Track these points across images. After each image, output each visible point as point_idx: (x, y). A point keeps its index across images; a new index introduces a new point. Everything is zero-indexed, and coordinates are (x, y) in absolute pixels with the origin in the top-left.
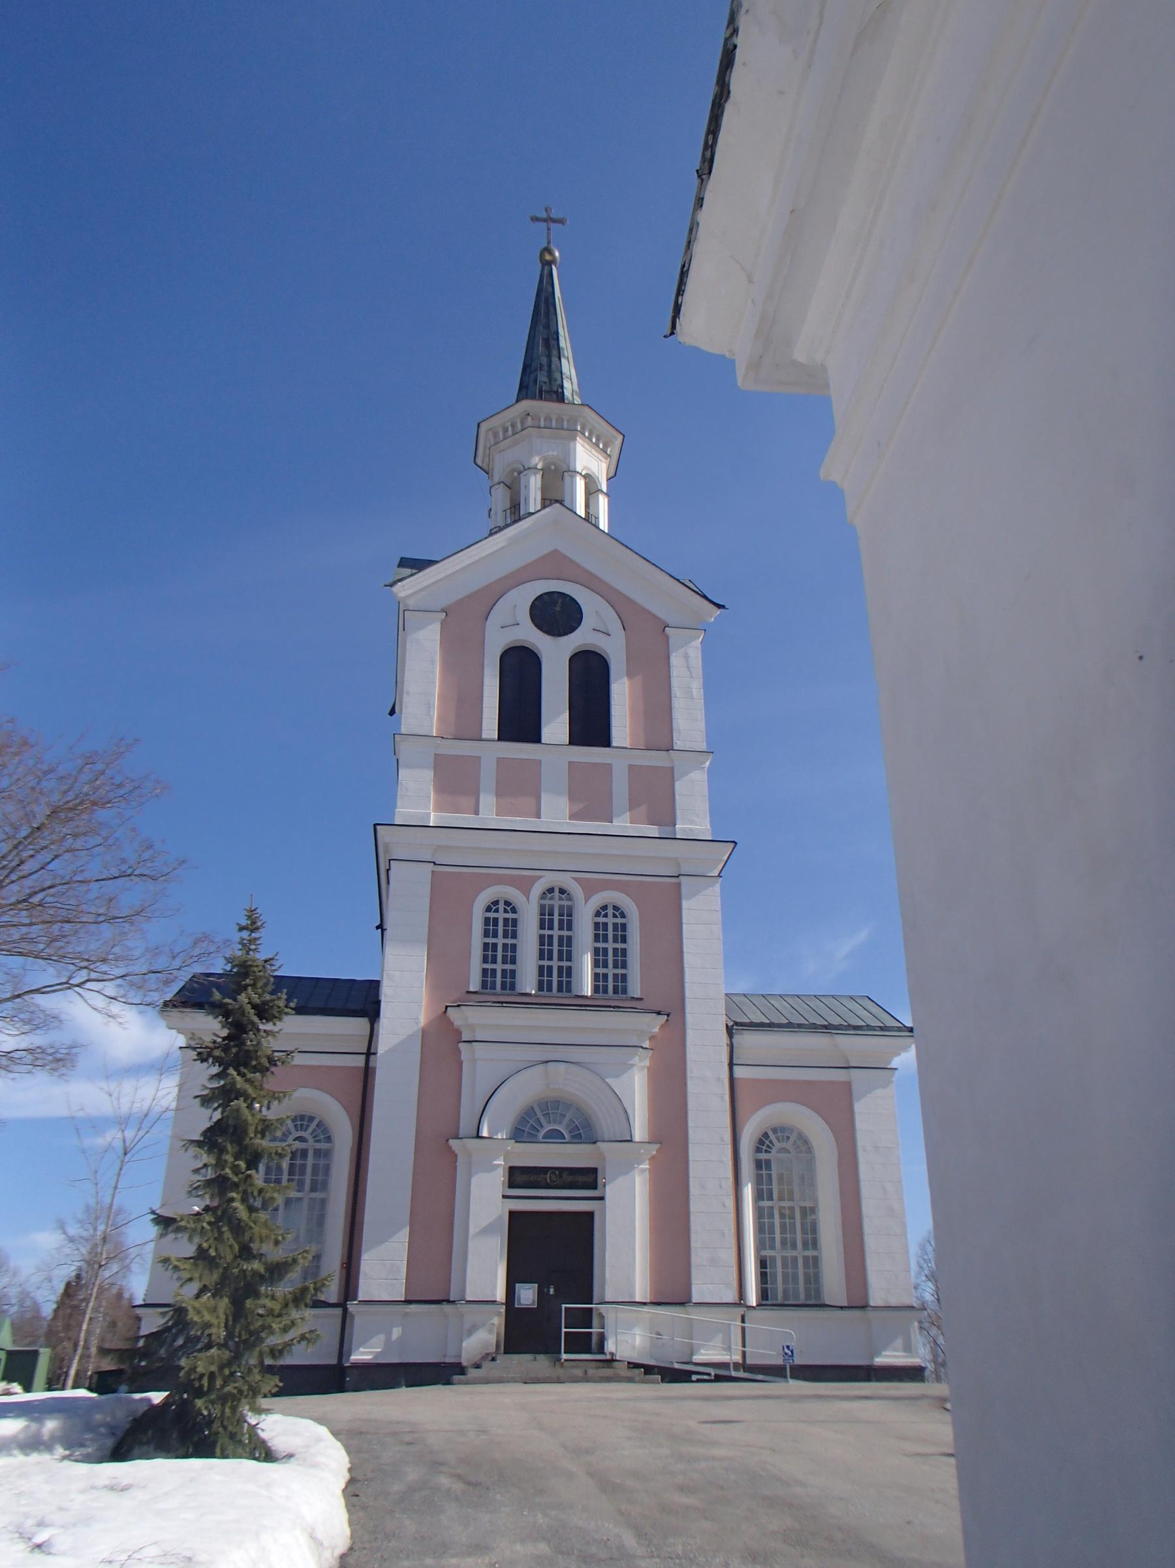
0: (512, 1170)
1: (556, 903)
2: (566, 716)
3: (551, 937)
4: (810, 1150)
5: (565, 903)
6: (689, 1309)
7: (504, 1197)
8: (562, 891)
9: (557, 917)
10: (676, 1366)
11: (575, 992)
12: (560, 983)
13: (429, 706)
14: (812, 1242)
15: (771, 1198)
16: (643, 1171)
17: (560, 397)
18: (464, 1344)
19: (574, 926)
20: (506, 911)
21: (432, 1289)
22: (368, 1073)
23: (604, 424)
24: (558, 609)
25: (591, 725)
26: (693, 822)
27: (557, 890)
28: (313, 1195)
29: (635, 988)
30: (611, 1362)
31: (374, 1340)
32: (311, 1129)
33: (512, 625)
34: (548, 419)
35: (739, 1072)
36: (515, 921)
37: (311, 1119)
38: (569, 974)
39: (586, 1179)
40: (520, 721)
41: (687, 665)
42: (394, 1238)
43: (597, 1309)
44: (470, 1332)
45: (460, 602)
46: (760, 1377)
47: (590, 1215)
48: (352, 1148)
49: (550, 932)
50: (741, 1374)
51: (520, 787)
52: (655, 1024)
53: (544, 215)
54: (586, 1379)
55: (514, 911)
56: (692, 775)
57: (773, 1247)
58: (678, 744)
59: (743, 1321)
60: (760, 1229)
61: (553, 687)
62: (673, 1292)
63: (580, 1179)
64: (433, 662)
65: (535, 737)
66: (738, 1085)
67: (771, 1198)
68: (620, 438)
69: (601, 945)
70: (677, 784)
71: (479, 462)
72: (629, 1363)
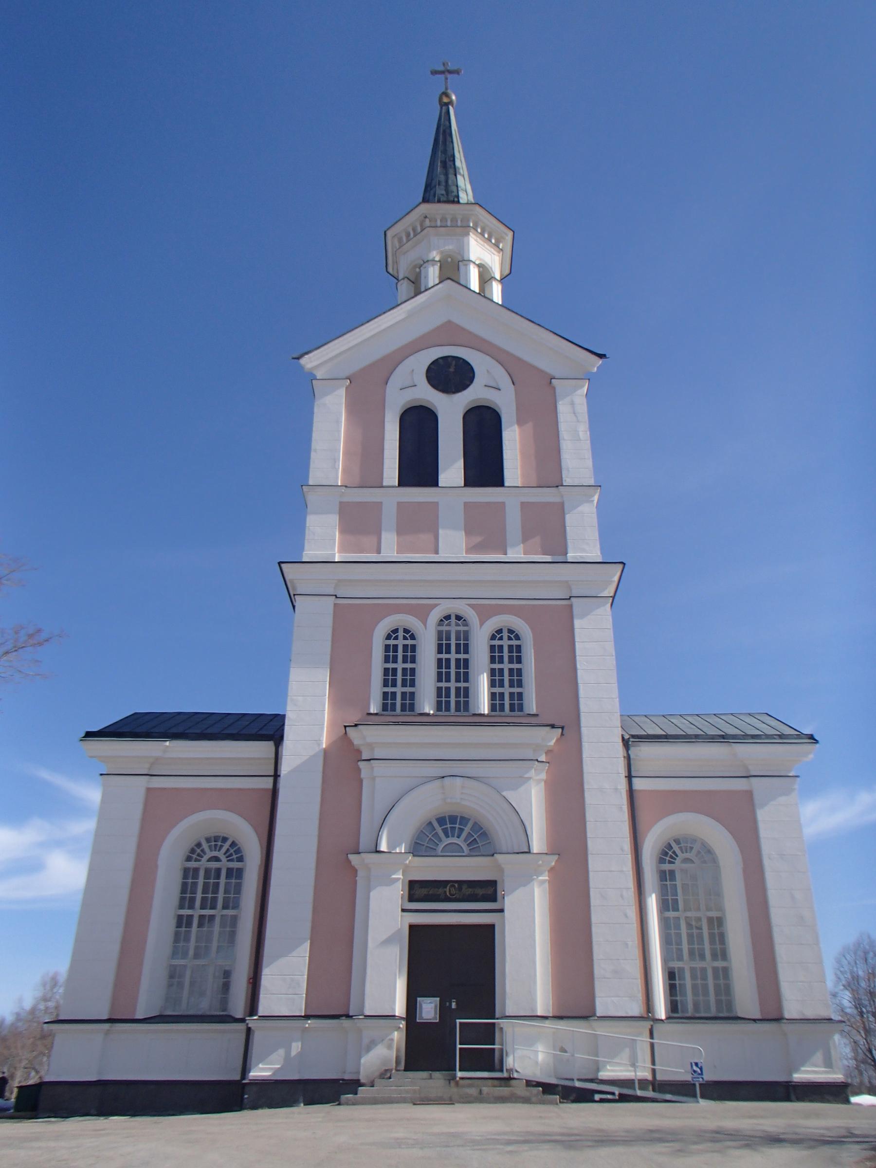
0: (412, 884)
1: (453, 629)
2: (461, 463)
3: (448, 689)
4: (715, 861)
5: (462, 628)
6: (595, 1024)
7: (403, 910)
8: (458, 618)
9: (454, 645)
10: (578, 1084)
11: (472, 710)
12: (458, 703)
13: (335, 460)
14: (722, 953)
15: (676, 909)
16: (543, 882)
17: (456, 201)
18: (363, 1061)
19: (471, 649)
20: (405, 638)
21: (333, 1003)
22: (275, 792)
23: (495, 222)
24: (452, 370)
25: (484, 467)
26: (584, 550)
27: (453, 617)
28: (225, 912)
29: (531, 704)
30: (508, 1080)
31: (274, 1056)
32: (224, 849)
33: (411, 386)
34: (444, 219)
35: (638, 784)
36: (414, 647)
37: (225, 839)
38: (466, 695)
39: (486, 891)
40: (419, 467)
41: (573, 413)
42: (294, 953)
43: (499, 1024)
44: (369, 1049)
45: (364, 370)
46: (668, 1097)
47: (491, 927)
48: (260, 866)
49: (447, 656)
50: (650, 1094)
51: (420, 524)
52: (551, 738)
53: (441, 68)
54: (481, 1099)
55: (413, 637)
56: (580, 508)
57: (680, 958)
58: (567, 481)
59: (652, 1036)
60: (666, 941)
61: (449, 438)
62: (576, 1004)
63: (480, 892)
64: (338, 422)
65: (432, 480)
66: (640, 802)
67: (676, 909)
68: (510, 234)
69: (497, 666)
70: (567, 517)
71: (390, 270)
72: (527, 1081)
